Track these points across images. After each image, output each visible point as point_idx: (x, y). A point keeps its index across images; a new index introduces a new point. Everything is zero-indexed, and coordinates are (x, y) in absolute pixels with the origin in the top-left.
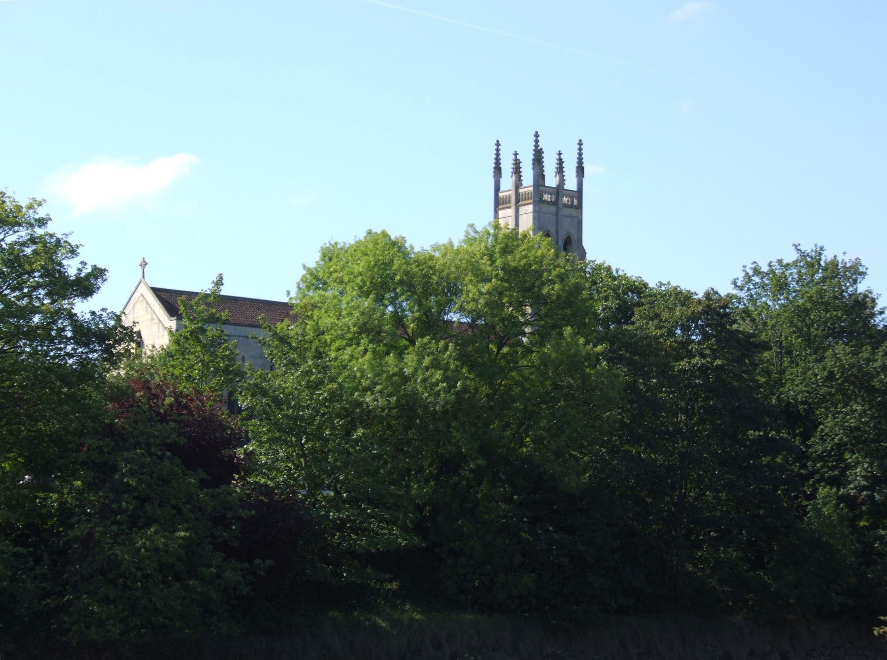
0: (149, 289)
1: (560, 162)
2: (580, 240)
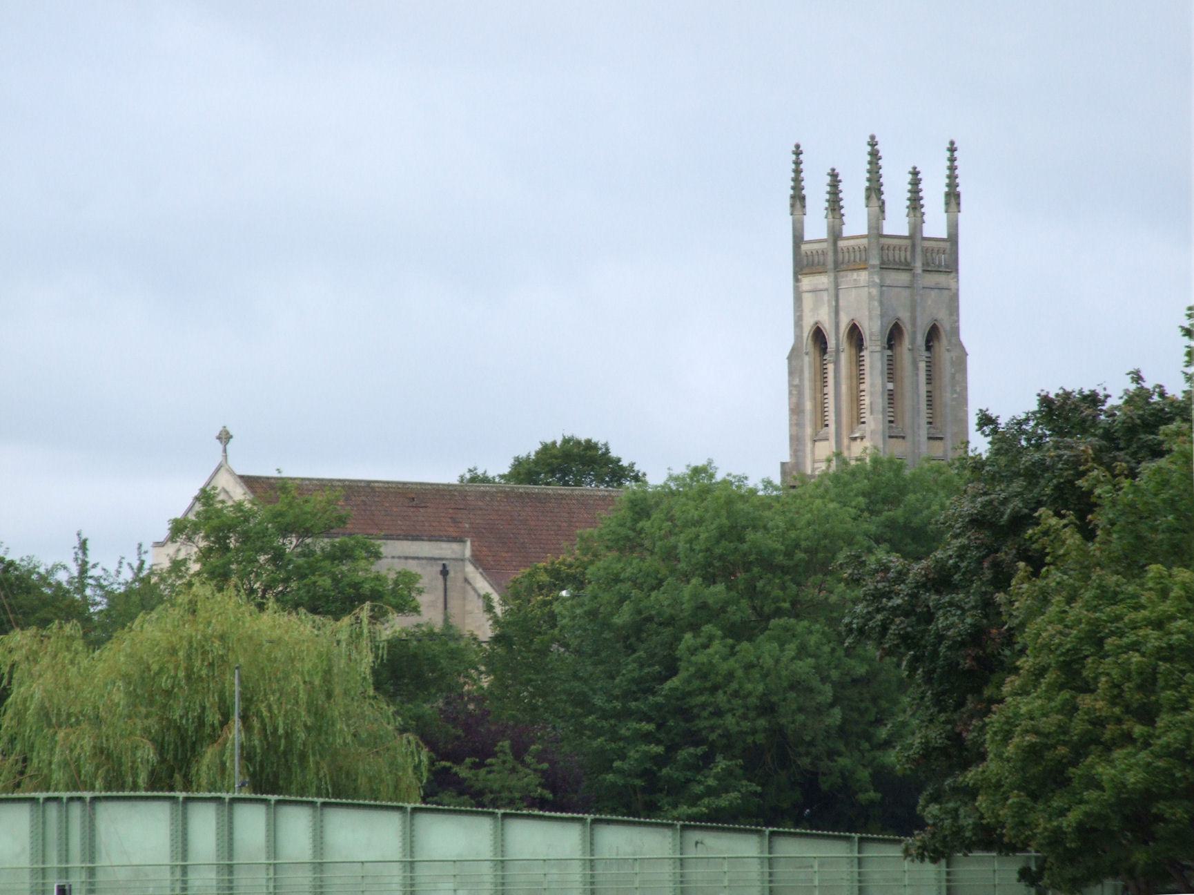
0: (239, 480)
1: (916, 177)
2: (955, 331)
